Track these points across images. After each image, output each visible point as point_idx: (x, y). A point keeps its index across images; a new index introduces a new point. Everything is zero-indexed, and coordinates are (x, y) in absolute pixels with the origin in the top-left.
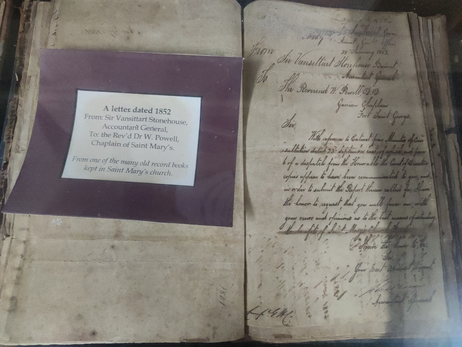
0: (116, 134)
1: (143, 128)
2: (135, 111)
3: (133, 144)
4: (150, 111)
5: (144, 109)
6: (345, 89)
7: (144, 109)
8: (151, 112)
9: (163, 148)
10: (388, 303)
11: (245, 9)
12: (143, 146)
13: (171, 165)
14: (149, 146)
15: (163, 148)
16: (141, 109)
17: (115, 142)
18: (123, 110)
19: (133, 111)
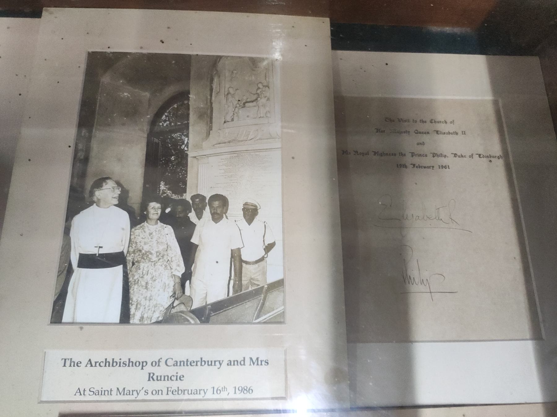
0: (152, 375)
1: (170, 362)
2: (145, 364)
3: (92, 390)
4: (242, 363)
5: (190, 360)
6: (146, 392)
7: (190, 360)
8: (244, 364)
9: (217, 363)
10: (416, 342)
11: (77, 220)
12: (106, 392)
13: (248, 361)
14: (248, 361)
15: (217, 363)
16: (185, 361)
17: (100, 390)
18: (189, 363)
19: (146, 362)
